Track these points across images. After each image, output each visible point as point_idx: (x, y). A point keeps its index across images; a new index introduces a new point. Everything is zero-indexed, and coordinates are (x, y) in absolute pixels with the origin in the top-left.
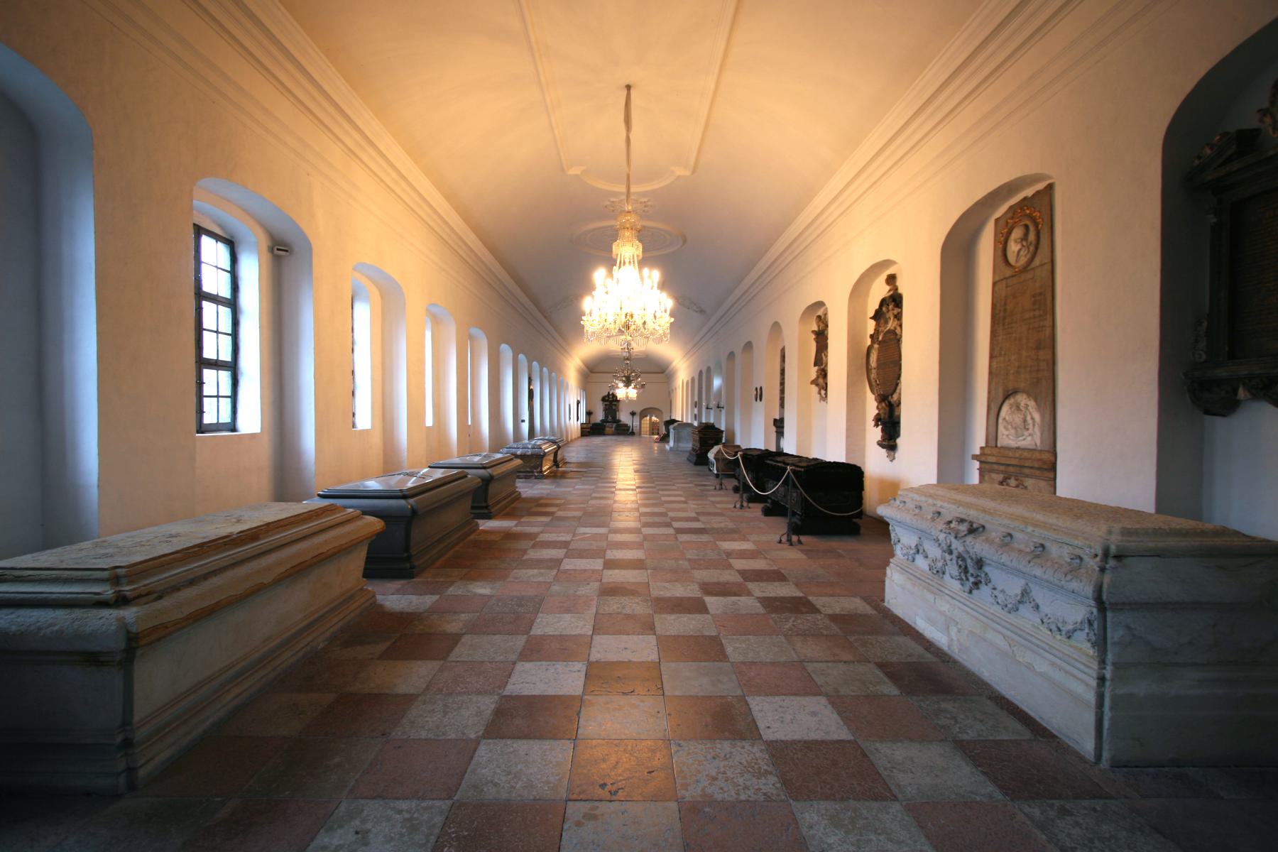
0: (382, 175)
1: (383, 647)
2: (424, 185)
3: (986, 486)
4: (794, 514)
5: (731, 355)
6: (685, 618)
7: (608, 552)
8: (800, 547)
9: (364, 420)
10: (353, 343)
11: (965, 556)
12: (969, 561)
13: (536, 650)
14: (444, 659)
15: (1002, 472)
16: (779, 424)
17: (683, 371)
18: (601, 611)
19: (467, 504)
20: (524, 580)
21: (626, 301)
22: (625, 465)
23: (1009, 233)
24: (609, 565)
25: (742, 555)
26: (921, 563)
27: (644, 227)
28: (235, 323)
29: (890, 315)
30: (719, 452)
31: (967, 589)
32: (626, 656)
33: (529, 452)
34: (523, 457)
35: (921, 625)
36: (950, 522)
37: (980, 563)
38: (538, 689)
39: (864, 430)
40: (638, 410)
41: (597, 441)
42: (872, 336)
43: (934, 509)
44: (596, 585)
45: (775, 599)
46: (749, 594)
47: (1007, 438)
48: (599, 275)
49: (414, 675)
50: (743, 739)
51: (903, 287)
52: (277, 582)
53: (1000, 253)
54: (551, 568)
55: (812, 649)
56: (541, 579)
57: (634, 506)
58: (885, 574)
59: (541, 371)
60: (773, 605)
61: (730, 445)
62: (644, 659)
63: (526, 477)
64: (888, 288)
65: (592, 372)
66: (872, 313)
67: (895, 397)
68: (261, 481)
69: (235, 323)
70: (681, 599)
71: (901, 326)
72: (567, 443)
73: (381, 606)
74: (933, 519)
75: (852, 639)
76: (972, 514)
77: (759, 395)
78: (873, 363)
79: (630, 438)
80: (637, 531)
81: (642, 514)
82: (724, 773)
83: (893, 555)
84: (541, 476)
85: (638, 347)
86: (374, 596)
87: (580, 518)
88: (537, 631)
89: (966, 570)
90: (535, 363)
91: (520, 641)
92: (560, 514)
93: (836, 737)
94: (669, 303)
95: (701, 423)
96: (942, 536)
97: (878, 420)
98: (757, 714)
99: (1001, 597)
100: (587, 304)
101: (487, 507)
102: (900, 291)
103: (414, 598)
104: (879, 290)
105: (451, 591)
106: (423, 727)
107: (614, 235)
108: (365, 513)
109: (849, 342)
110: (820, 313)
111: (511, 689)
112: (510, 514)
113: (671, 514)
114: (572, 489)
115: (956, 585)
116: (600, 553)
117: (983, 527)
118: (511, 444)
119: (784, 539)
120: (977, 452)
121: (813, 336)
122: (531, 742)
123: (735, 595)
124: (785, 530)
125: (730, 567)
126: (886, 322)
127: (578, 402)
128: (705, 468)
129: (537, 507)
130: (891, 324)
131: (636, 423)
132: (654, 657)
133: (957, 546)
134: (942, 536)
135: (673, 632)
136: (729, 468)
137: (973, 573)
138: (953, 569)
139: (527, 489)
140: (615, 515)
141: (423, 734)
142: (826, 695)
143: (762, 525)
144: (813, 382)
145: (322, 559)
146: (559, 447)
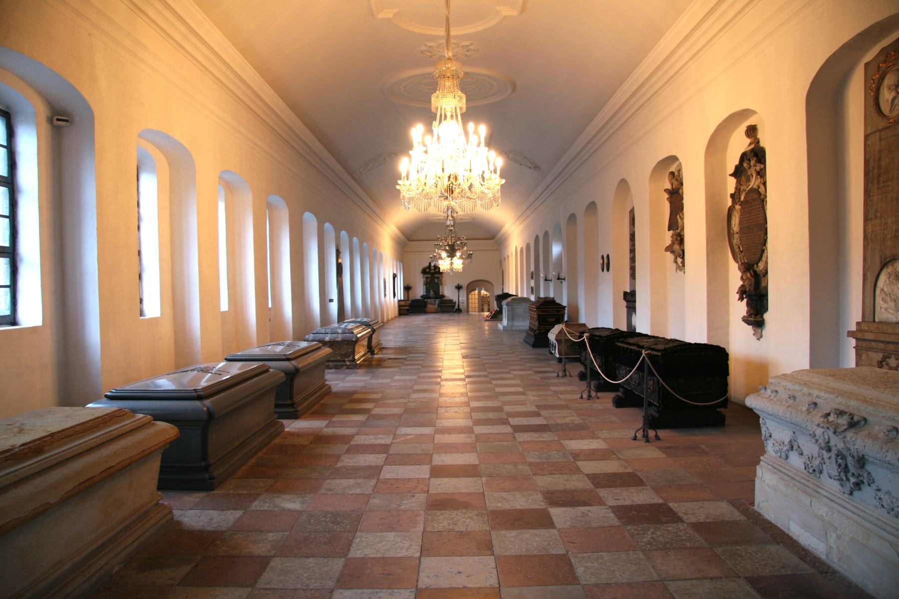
1: (184, 571)
2: (216, 38)
3: (865, 370)
4: (650, 404)
5: (572, 218)
6: (528, 534)
7: (435, 457)
8: (658, 443)
9: (153, 307)
10: (139, 219)
11: (845, 453)
12: (849, 459)
14: (252, 585)
15: (881, 350)
16: (630, 298)
17: (516, 237)
18: (429, 529)
19: (271, 400)
20: (339, 491)
21: (449, 161)
22: (452, 348)
23: (882, 78)
24: (438, 472)
25: (592, 455)
26: (796, 461)
27: (466, 74)
28: (13, 204)
29: (752, 172)
30: (561, 332)
31: (847, 490)
32: (460, 581)
33: (340, 338)
34: (332, 344)
35: (796, 531)
36: (828, 414)
37: (862, 461)
39: (727, 303)
40: (464, 283)
41: (418, 320)
42: (732, 196)
43: (809, 399)
44: (422, 497)
46: (601, 502)
47: (885, 312)
48: (417, 131)
51: (766, 141)
52: (67, 500)
53: (871, 101)
54: (369, 477)
55: (673, 565)
56: (358, 491)
58: (754, 473)
59: (351, 242)
60: (628, 515)
61: (573, 323)
62: (481, 585)
63: (336, 367)
64: (748, 141)
66: (731, 170)
67: (761, 265)
68: (44, 381)
69: (13, 204)
70: (522, 512)
71: (765, 184)
72: (384, 324)
73: (179, 523)
74: (809, 411)
75: (719, 550)
76: (853, 405)
77: (606, 265)
78: (735, 228)
79: (456, 317)
80: (468, 430)
81: (473, 410)
83: (762, 451)
84: (354, 366)
86: (171, 512)
87: (400, 416)
88: (356, 553)
89: (846, 469)
90: (343, 233)
91: (337, 565)
92: (377, 411)
94: (499, 162)
96: (819, 432)
97: (742, 293)
99: (886, 499)
100: (404, 165)
101: (292, 405)
102: (762, 144)
103: (214, 513)
104: (739, 144)
105: (256, 505)
107: (433, 85)
109: (706, 193)
110: (673, 169)
112: (319, 413)
113: (507, 408)
114: (389, 381)
115: (835, 486)
116: (423, 458)
117: (865, 420)
118: (318, 329)
119: (640, 435)
120: (853, 328)
121: (666, 196)
123: (585, 504)
124: (640, 425)
125: (578, 471)
126: (748, 180)
127: (395, 276)
128: (544, 351)
129: (350, 402)
130: (754, 182)
131: (463, 298)
132: (493, 581)
133: (836, 442)
134: (819, 432)
135: (513, 551)
136: (573, 351)
137: (854, 472)
138: (831, 468)
139: (339, 381)
140: (442, 411)
143: (614, 418)
144: (667, 249)
145: (112, 473)
146: (374, 331)
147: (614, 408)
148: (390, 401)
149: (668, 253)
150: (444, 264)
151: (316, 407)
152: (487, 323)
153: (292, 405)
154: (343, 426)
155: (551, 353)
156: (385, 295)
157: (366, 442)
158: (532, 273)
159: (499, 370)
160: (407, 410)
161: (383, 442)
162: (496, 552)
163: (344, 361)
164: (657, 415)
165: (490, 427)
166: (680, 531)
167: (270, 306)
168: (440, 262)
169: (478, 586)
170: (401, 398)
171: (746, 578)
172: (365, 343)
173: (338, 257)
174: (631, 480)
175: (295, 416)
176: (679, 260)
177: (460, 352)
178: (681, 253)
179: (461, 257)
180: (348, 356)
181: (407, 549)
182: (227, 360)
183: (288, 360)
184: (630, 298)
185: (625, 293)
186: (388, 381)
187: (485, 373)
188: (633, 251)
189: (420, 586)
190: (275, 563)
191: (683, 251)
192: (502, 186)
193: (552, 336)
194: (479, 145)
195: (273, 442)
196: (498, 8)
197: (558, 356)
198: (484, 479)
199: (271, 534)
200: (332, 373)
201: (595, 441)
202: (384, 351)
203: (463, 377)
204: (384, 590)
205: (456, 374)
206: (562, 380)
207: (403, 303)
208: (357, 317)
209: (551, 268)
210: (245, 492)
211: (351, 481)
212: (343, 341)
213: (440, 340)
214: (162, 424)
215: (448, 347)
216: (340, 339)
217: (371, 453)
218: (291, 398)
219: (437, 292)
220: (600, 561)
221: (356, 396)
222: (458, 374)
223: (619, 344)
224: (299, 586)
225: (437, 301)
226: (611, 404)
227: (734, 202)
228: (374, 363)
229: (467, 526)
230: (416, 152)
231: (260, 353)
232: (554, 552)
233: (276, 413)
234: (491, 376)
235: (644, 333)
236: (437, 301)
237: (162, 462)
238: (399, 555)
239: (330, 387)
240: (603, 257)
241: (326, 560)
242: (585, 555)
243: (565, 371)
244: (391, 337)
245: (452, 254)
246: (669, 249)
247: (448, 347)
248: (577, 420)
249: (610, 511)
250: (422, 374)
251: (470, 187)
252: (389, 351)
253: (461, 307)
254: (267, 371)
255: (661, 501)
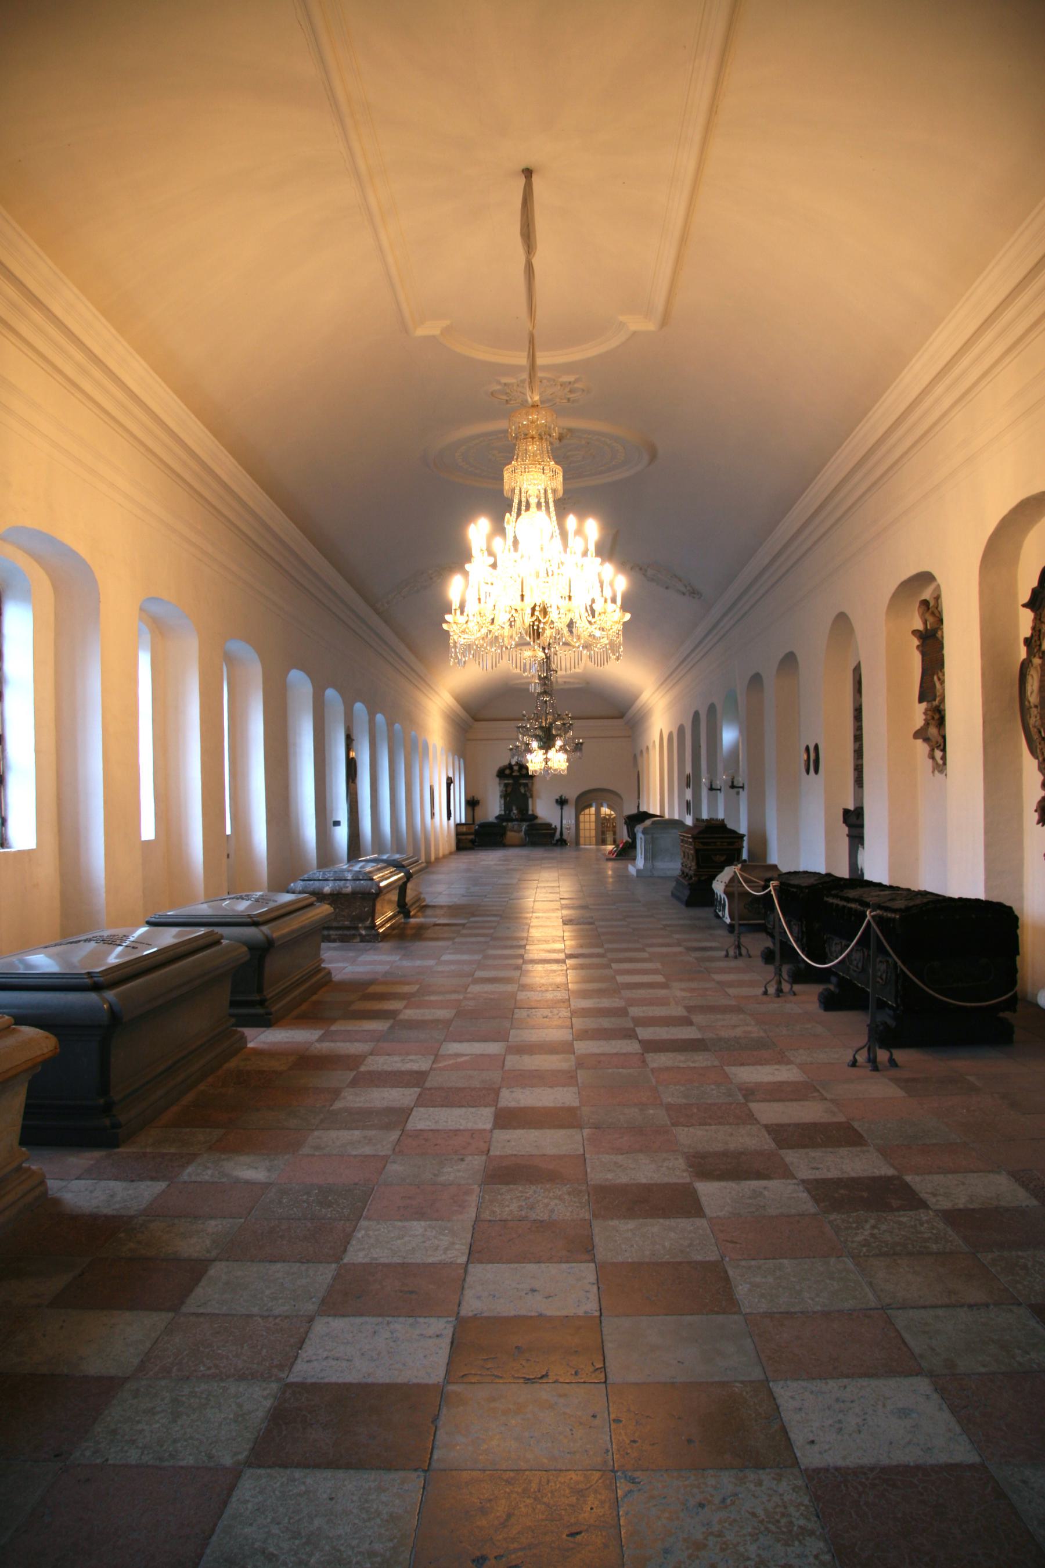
0: (58, 361)
2: (136, 372)
4: (881, 1005)
5: (756, 681)
6: (656, 1227)
7: (505, 1093)
8: (894, 1072)
13: (356, 1293)
17: (661, 715)
18: (486, 1215)
20: (336, 1148)
21: (535, 580)
22: (548, 909)
25: (777, 1092)
30: (733, 879)
33: (349, 888)
34: (335, 898)
38: (356, 1370)
40: (572, 795)
41: (490, 859)
42: (1027, 642)
44: (476, 1162)
45: (838, 1183)
46: (787, 1173)
48: (478, 531)
49: (118, 1341)
50: (759, 1466)
54: (388, 1127)
56: (368, 1150)
57: (561, 995)
60: (832, 1194)
61: (759, 865)
62: (570, 1312)
63: (344, 939)
65: (476, 720)
66: (1025, 596)
72: (429, 865)
73: (56, 1202)
77: (813, 762)
79: (557, 852)
80: (566, 1048)
81: (585, 1013)
82: (720, 1535)
84: (374, 937)
85: (569, 665)
86: (43, 1182)
87: (447, 1023)
88: (356, 1255)
90: (359, 707)
91: (324, 1275)
92: (409, 1014)
93: (943, 1458)
94: (621, 583)
95: (698, 820)
98: (788, 1416)
100: (455, 588)
101: (262, 1003)
105: (190, 1173)
106: (133, 1442)
107: (503, 452)
108: (21, 1020)
110: (927, 594)
111: (304, 1370)
113: (635, 1011)
114: (440, 963)
116: (487, 1095)
118: (314, 871)
119: (861, 1058)
121: (916, 642)
122: (341, 1474)
123: (759, 1176)
124: (864, 1040)
125: (750, 1118)
127: (450, 782)
128: (706, 912)
129: (365, 999)
131: (569, 821)
132: (590, 1306)
136: (753, 914)
139: (343, 963)
140: (520, 1014)
141: (133, 1456)
142: (931, 1375)
144: (917, 735)
146: (409, 877)
147: (821, 1012)
148: (433, 998)
149: (919, 741)
150: (535, 761)
151: (304, 1007)
152: (610, 864)
153: (262, 1003)
154: (349, 1038)
155: (718, 916)
156: (433, 815)
157: (387, 1068)
158: (688, 777)
159: (624, 946)
160: (461, 1014)
161: (415, 1067)
162: (599, 1257)
163: (356, 928)
164: (892, 1023)
165: (602, 1043)
166: (922, 1225)
167: (228, 832)
168: (529, 757)
169: (564, 1313)
170: (455, 992)
171: (1031, 1306)
172: (394, 896)
173: (349, 748)
174: (843, 1135)
175: (266, 1022)
176: (938, 754)
177: (559, 914)
178: (941, 741)
179: (563, 749)
180: (362, 920)
181: (446, 1249)
182: (150, 923)
183: (255, 924)
184: (853, 819)
185: (846, 812)
186: (431, 963)
187: (600, 951)
188: (858, 738)
189: (463, 1313)
190: (218, 1270)
191: (944, 737)
192: (625, 624)
193: (719, 886)
194: (585, 554)
195: (226, 1066)
196: (621, 318)
197: (728, 921)
198: (586, 1132)
199: (213, 1223)
200: (335, 949)
201: (783, 1068)
202: (429, 912)
203: (562, 956)
204: (401, 1319)
205: (549, 951)
206: (733, 964)
207: (464, 829)
208: (380, 852)
209: (720, 767)
210: (173, 1150)
211: (357, 1132)
212: (354, 894)
213: (528, 893)
214: (29, 1031)
215: (538, 905)
216: (349, 890)
217: (393, 1086)
218: (260, 990)
219: (523, 809)
220: (778, 1273)
221: (372, 989)
222: (554, 951)
223: (830, 900)
224: (255, 1310)
225: (524, 826)
226: (817, 1005)
227: (1030, 653)
228: (409, 932)
229: (552, 1211)
230: (478, 565)
231: (210, 912)
232: (699, 1258)
233: (232, 1016)
234: (610, 955)
235: (876, 880)
236: (524, 826)
237: (28, 1097)
238: (430, 1260)
239: (329, 973)
240: (807, 749)
241: (304, 1267)
242: (753, 1263)
243: (739, 947)
244: (440, 888)
245: (547, 743)
246: (920, 734)
247: (538, 905)
248: (755, 1031)
249: (801, 1188)
250: (491, 952)
251: (571, 625)
252: (439, 912)
253: (565, 837)
254: (218, 942)
255: (890, 1172)
